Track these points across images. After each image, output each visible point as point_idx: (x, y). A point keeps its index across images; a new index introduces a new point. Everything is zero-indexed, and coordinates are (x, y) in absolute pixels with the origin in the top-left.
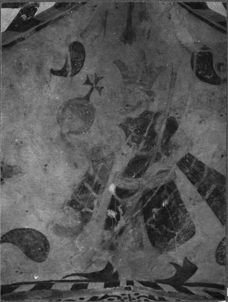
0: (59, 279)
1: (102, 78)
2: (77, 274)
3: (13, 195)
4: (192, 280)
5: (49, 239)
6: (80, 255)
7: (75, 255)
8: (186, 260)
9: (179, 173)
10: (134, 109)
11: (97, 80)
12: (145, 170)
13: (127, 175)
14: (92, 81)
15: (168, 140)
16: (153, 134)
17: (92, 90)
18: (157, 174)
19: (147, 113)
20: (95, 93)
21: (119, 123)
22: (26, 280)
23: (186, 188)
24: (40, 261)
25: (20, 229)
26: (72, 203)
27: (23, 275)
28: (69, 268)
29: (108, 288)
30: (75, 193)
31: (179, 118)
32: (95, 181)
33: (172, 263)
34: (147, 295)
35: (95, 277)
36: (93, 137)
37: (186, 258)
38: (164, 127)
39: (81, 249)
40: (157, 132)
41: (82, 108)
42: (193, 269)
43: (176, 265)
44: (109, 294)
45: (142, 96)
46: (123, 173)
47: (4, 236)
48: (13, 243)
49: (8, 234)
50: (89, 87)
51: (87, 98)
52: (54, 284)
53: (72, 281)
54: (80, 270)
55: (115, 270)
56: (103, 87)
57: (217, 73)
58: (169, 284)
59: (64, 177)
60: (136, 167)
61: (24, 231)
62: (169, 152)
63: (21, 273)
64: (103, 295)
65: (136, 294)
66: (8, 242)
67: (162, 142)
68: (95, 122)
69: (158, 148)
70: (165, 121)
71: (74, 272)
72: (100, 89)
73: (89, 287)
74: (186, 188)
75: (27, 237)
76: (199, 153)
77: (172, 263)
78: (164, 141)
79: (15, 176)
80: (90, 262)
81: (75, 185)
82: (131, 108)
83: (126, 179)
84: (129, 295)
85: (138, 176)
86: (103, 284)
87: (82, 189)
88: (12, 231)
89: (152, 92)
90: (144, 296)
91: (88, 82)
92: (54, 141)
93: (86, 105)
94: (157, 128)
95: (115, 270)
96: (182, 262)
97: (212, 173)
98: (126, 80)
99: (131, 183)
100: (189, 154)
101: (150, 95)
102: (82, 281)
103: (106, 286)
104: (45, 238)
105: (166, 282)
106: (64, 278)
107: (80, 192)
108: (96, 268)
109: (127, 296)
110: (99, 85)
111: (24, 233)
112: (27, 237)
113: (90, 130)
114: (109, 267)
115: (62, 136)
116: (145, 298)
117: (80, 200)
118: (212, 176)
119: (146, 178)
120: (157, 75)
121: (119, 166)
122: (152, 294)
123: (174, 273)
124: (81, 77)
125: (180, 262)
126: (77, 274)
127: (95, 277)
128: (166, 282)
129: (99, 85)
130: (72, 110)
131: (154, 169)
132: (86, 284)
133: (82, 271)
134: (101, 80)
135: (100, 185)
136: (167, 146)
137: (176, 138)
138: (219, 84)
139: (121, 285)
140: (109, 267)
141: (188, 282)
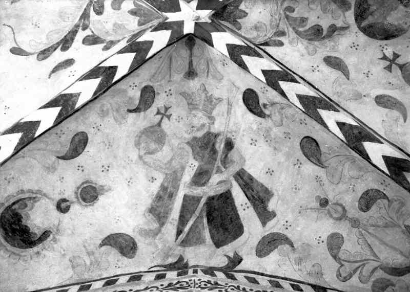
0: (146, 270)
1: (170, 108)
2: (158, 266)
3: (107, 208)
4: (238, 268)
5: (136, 240)
6: (160, 251)
7: (156, 251)
8: (236, 254)
9: (235, 184)
10: (198, 130)
11: (167, 109)
12: (208, 181)
13: (194, 184)
14: (163, 111)
15: (226, 156)
16: (214, 151)
17: (162, 119)
18: (217, 184)
19: (209, 133)
20: (165, 120)
21: (186, 141)
22: (124, 273)
23: (239, 197)
24: (131, 257)
25: (114, 234)
26: (152, 210)
27: (119, 269)
28: (152, 262)
29: (179, 277)
30: (154, 201)
31: (234, 139)
32: (169, 191)
33: (225, 255)
34: (206, 281)
35: (171, 267)
36: (165, 154)
37: (235, 252)
38: (222, 146)
39: (160, 246)
40: (218, 149)
41: (155, 134)
42: (240, 260)
43: (228, 257)
44: (181, 281)
45: (205, 120)
46: (190, 183)
47: (104, 240)
48: (111, 245)
49: (106, 238)
50: (159, 117)
51: (159, 124)
52: (142, 275)
53: (155, 271)
54: (159, 261)
55: (185, 261)
56: (171, 115)
57: (263, 109)
58: (221, 271)
59: (146, 190)
60: (201, 177)
61: (118, 236)
62: (227, 166)
63: (119, 267)
64: (176, 281)
65: (199, 280)
66: (107, 245)
67: (222, 157)
68: (167, 141)
69: (218, 163)
70: (224, 140)
71: (156, 264)
72: (169, 117)
73: (167, 276)
74: (239, 197)
75: (67, 96)
76: (249, 169)
77: (225, 255)
78: (223, 157)
79: (106, 193)
80: (167, 256)
81: (153, 195)
82: (195, 129)
83: (193, 187)
84: (194, 280)
85: (203, 185)
86: (175, 273)
87: (159, 198)
88: (109, 236)
89: (213, 117)
90: (205, 281)
91: (158, 113)
92: (134, 162)
93: (158, 130)
94: (217, 146)
95: (185, 261)
96: (233, 254)
97: (259, 185)
98: (191, 107)
99: (198, 191)
100: (243, 169)
101: (211, 120)
102: (162, 271)
103: (179, 275)
104: (133, 239)
105: (220, 269)
106: (149, 269)
107: (157, 201)
108: (171, 260)
109: (192, 282)
110: (168, 113)
111: (117, 237)
112: (120, 240)
113: (163, 149)
114: (181, 259)
115: (140, 157)
116: (205, 283)
117: (158, 211)
118: (259, 187)
119: (209, 187)
120: (216, 105)
121: (187, 177)
122: (210, 280)
123: (227, 263)
124: (153, 109)
125: (231, 255)
126: (158, 266)
127: (171, 267)
128: (220, 269)
129: (168, 113)
130: (148, 136)
131: (215, 178)
132: (163, 274)
133: (161, 263)
134: (170, 109)
135: (172, 194)
136: (225, 161)
137: (233, 155)
138: (264, 117)
139: (189, 274)
140: (181, 259)
141: (235, 269)
